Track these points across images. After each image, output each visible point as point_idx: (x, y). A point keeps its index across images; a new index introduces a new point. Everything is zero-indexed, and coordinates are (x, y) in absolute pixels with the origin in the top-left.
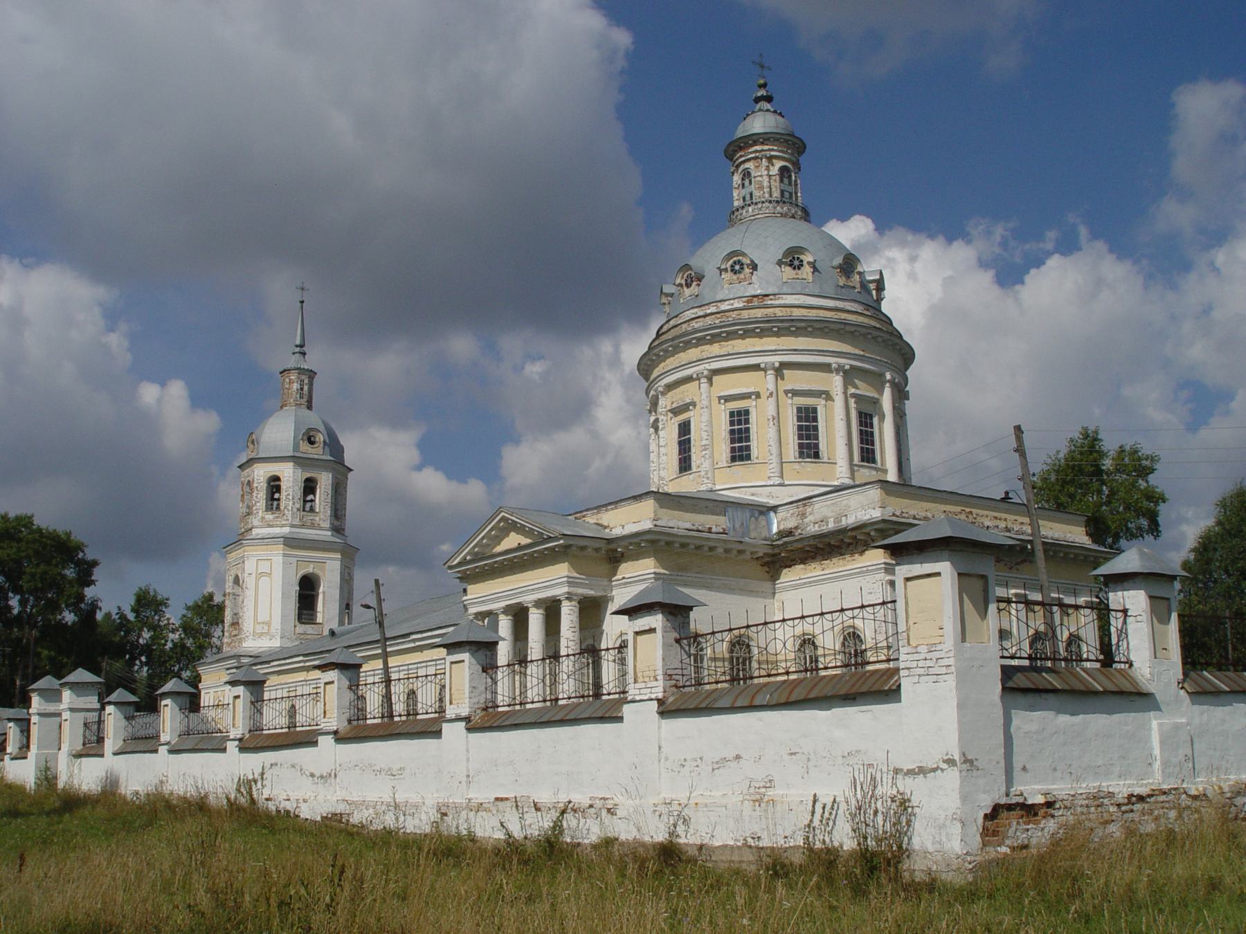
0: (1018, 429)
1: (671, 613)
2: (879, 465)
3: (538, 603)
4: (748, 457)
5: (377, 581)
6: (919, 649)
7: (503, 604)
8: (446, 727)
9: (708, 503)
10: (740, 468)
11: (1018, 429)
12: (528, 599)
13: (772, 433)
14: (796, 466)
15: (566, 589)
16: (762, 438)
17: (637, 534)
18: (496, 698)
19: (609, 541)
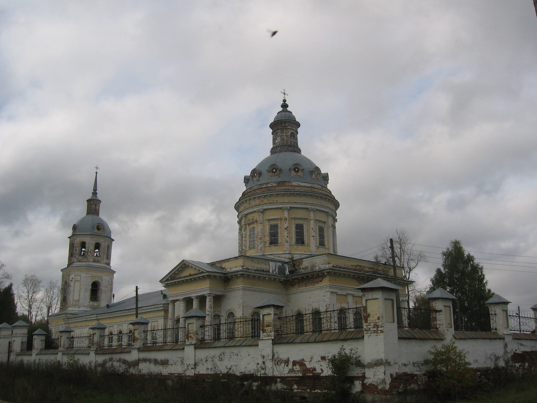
0: (391, 241)
1: (277, 309)
2: (326, 247)
3: (197, 297)
4: (277, 243)
5: (137, 287)
6: (371, 324)
7: (183, 297)
8: (186, 348)
9: (263, 260)
10: (273, 247)
11: (391, 241)
12: (193, 295)
13: (286, 235)
14: (295, 247)
15: (208, 292)
16: (283, 235)
17: (237, 272)
18: (204, 337)
19: (225, 274)
